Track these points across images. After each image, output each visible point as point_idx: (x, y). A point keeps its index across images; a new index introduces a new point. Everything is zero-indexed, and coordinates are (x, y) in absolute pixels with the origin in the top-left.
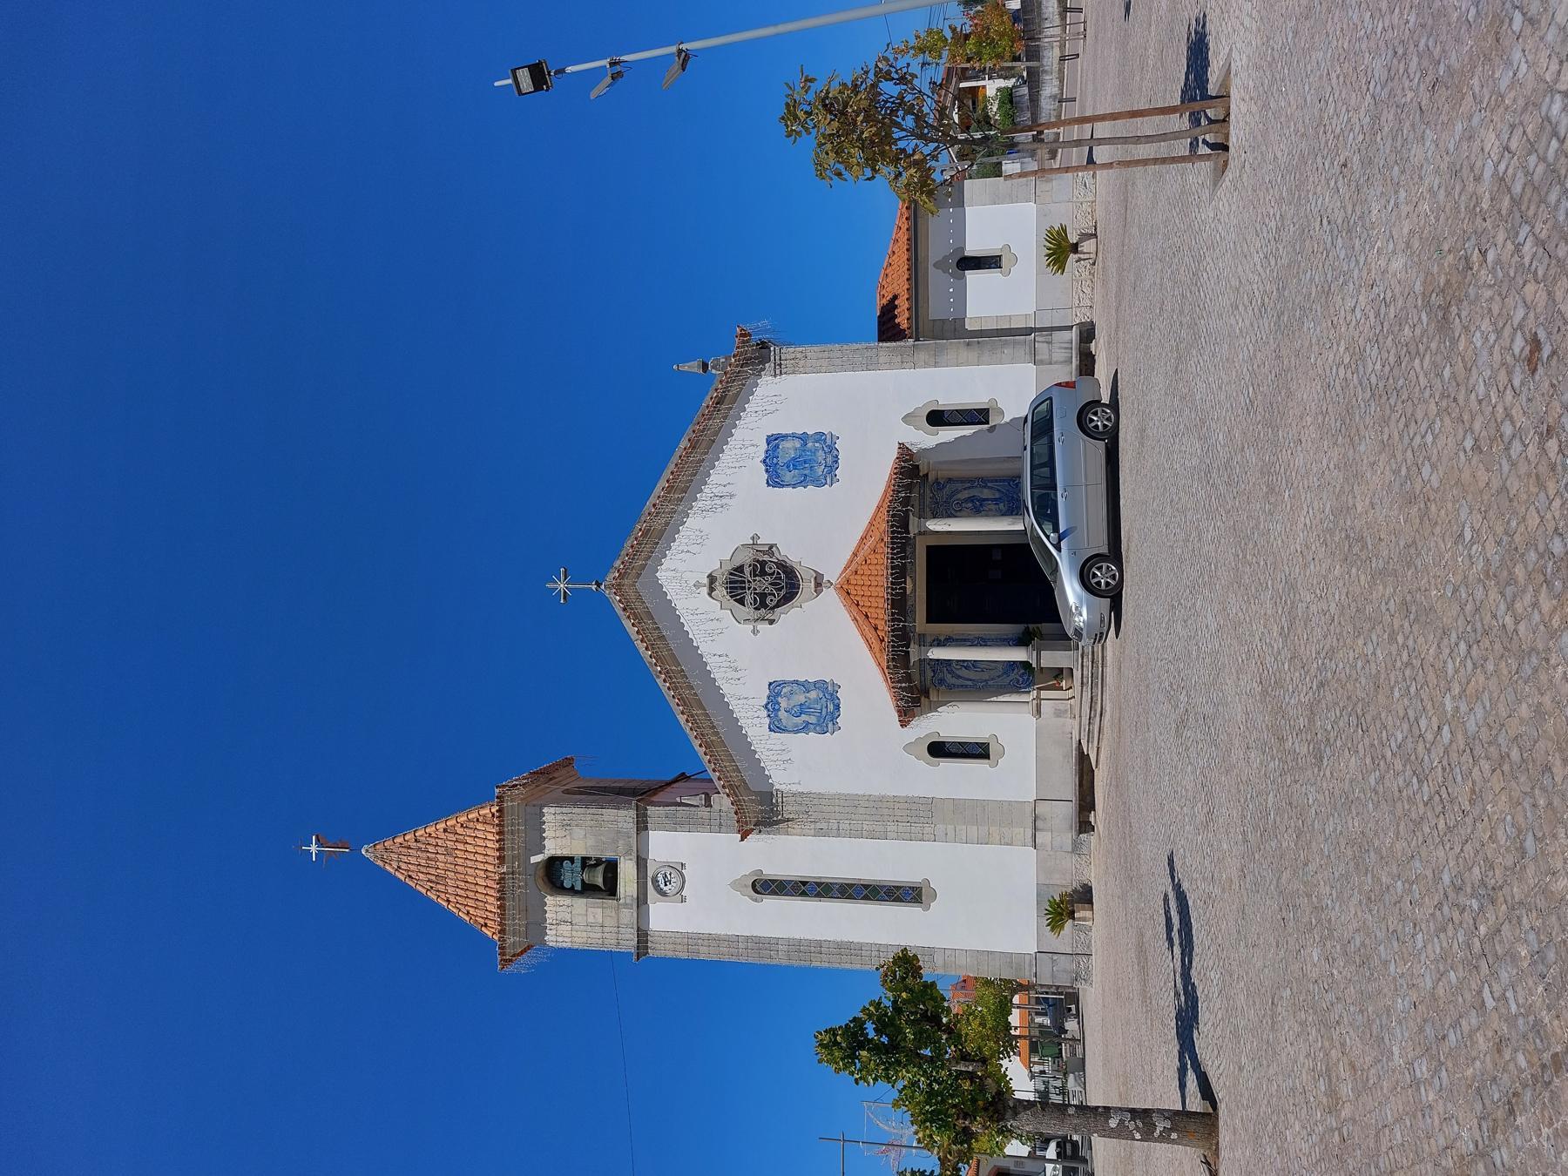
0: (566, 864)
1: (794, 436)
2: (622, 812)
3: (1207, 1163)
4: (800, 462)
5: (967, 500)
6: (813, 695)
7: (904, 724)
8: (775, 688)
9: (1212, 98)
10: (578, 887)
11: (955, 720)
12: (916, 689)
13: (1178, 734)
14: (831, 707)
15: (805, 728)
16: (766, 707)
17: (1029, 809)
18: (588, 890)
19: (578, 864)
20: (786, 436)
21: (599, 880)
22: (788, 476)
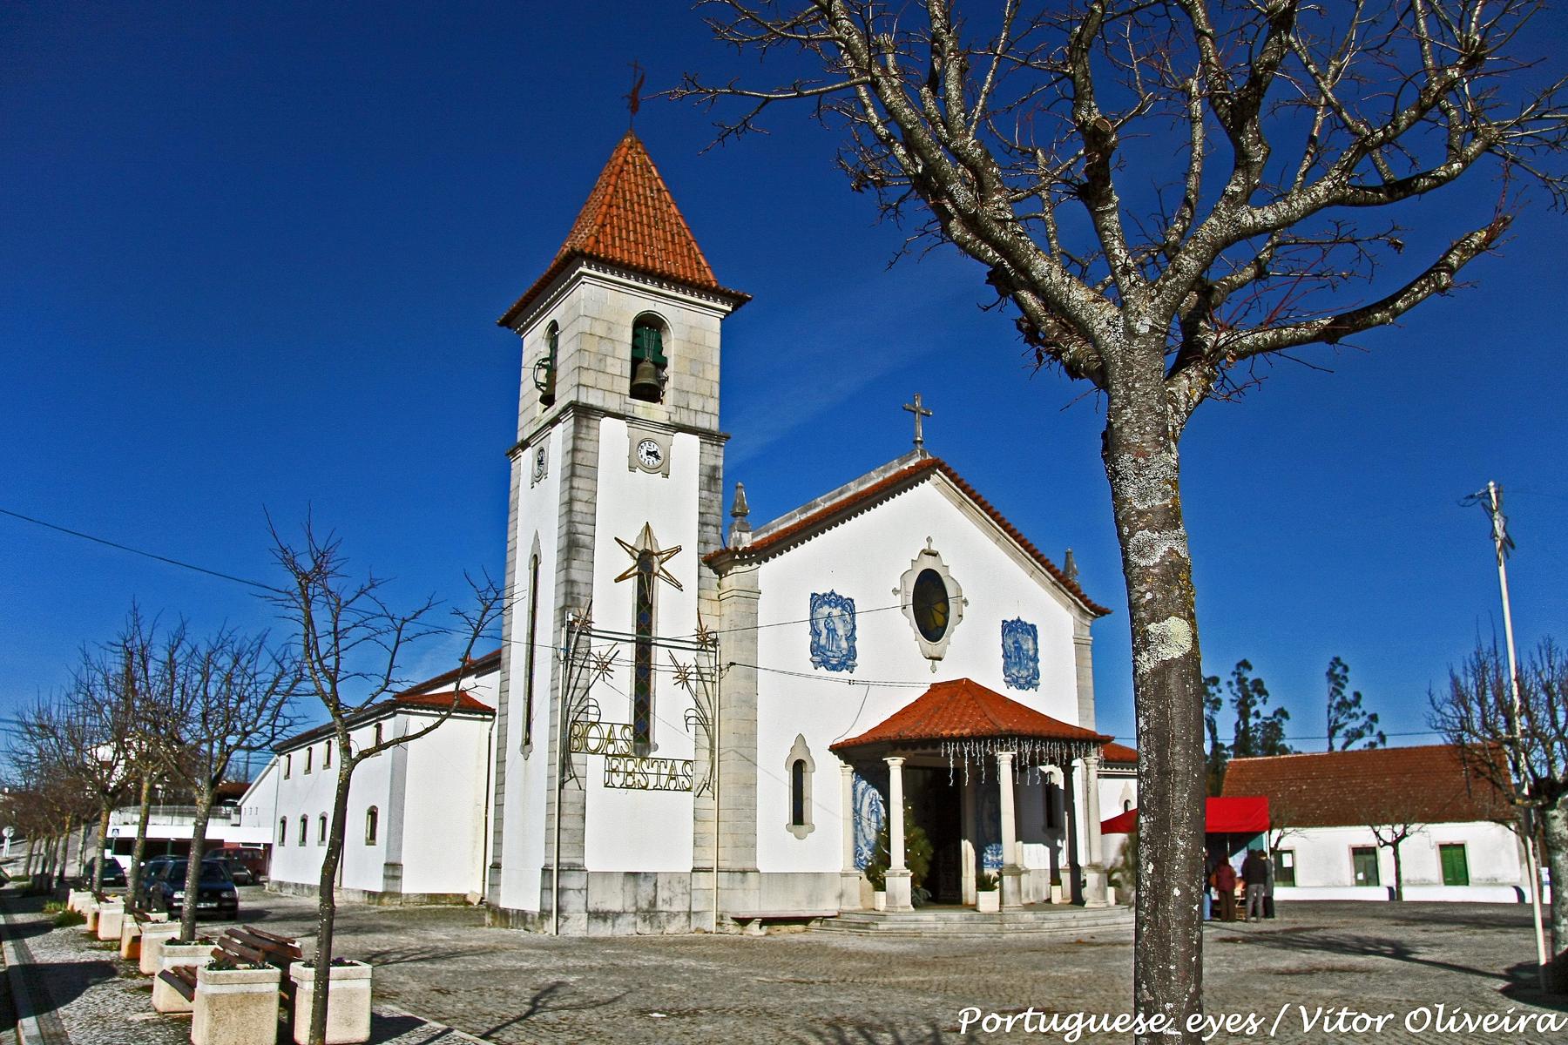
1: (1036, 650)
3: (703, 721)
6: (844, 644)
7: (837, 749)
8: (847, 605)
11: (832, 783)
12: (863, 756)
14: (834, 662)
15: (815, 633)
16: (832, 593)
17: (748, 865)
20: (1035, 643)
22: (1010, 642)
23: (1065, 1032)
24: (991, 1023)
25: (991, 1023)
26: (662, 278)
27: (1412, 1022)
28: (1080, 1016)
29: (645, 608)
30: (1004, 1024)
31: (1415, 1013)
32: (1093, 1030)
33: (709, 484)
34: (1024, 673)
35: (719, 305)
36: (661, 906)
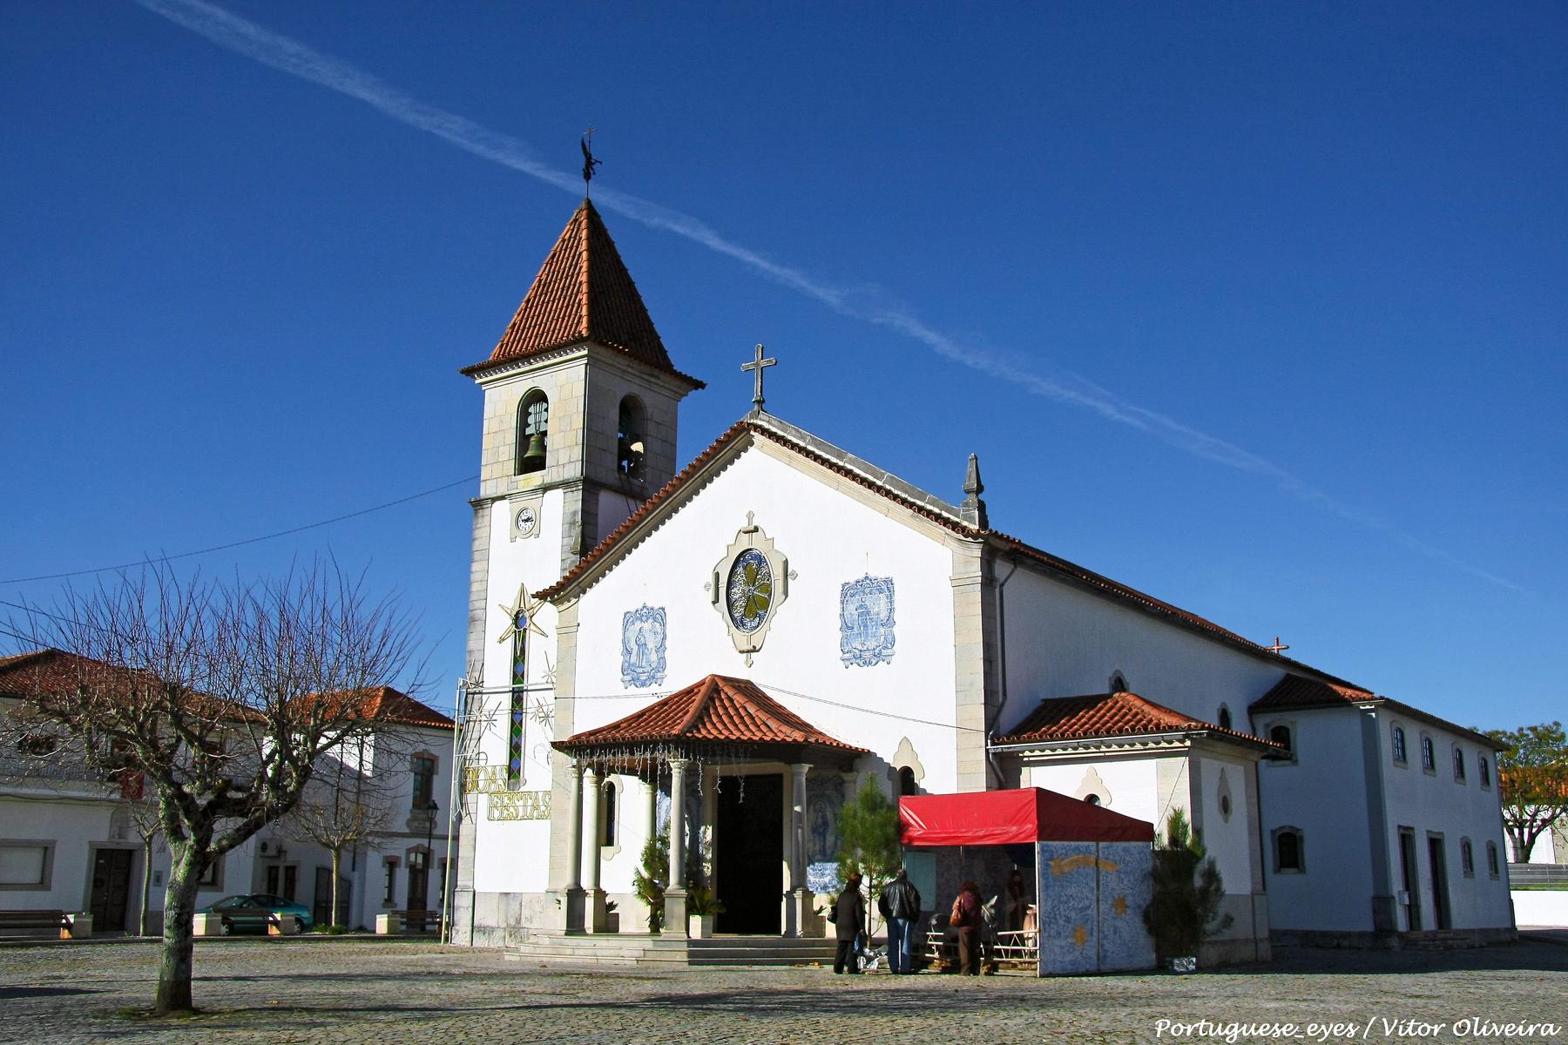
4: (866, 620)
5: (824, 817)
9: (197, 1011)
10: (529, 431)
14: (643, 677)
15: (627, 651)
18: (523, 440)
21: (531, 459)
24: (1177, 1030)
25: (1177, 1030)
26: (526, 357)
29: (519, 659)
34: (871, 644)
36: (524, 923)
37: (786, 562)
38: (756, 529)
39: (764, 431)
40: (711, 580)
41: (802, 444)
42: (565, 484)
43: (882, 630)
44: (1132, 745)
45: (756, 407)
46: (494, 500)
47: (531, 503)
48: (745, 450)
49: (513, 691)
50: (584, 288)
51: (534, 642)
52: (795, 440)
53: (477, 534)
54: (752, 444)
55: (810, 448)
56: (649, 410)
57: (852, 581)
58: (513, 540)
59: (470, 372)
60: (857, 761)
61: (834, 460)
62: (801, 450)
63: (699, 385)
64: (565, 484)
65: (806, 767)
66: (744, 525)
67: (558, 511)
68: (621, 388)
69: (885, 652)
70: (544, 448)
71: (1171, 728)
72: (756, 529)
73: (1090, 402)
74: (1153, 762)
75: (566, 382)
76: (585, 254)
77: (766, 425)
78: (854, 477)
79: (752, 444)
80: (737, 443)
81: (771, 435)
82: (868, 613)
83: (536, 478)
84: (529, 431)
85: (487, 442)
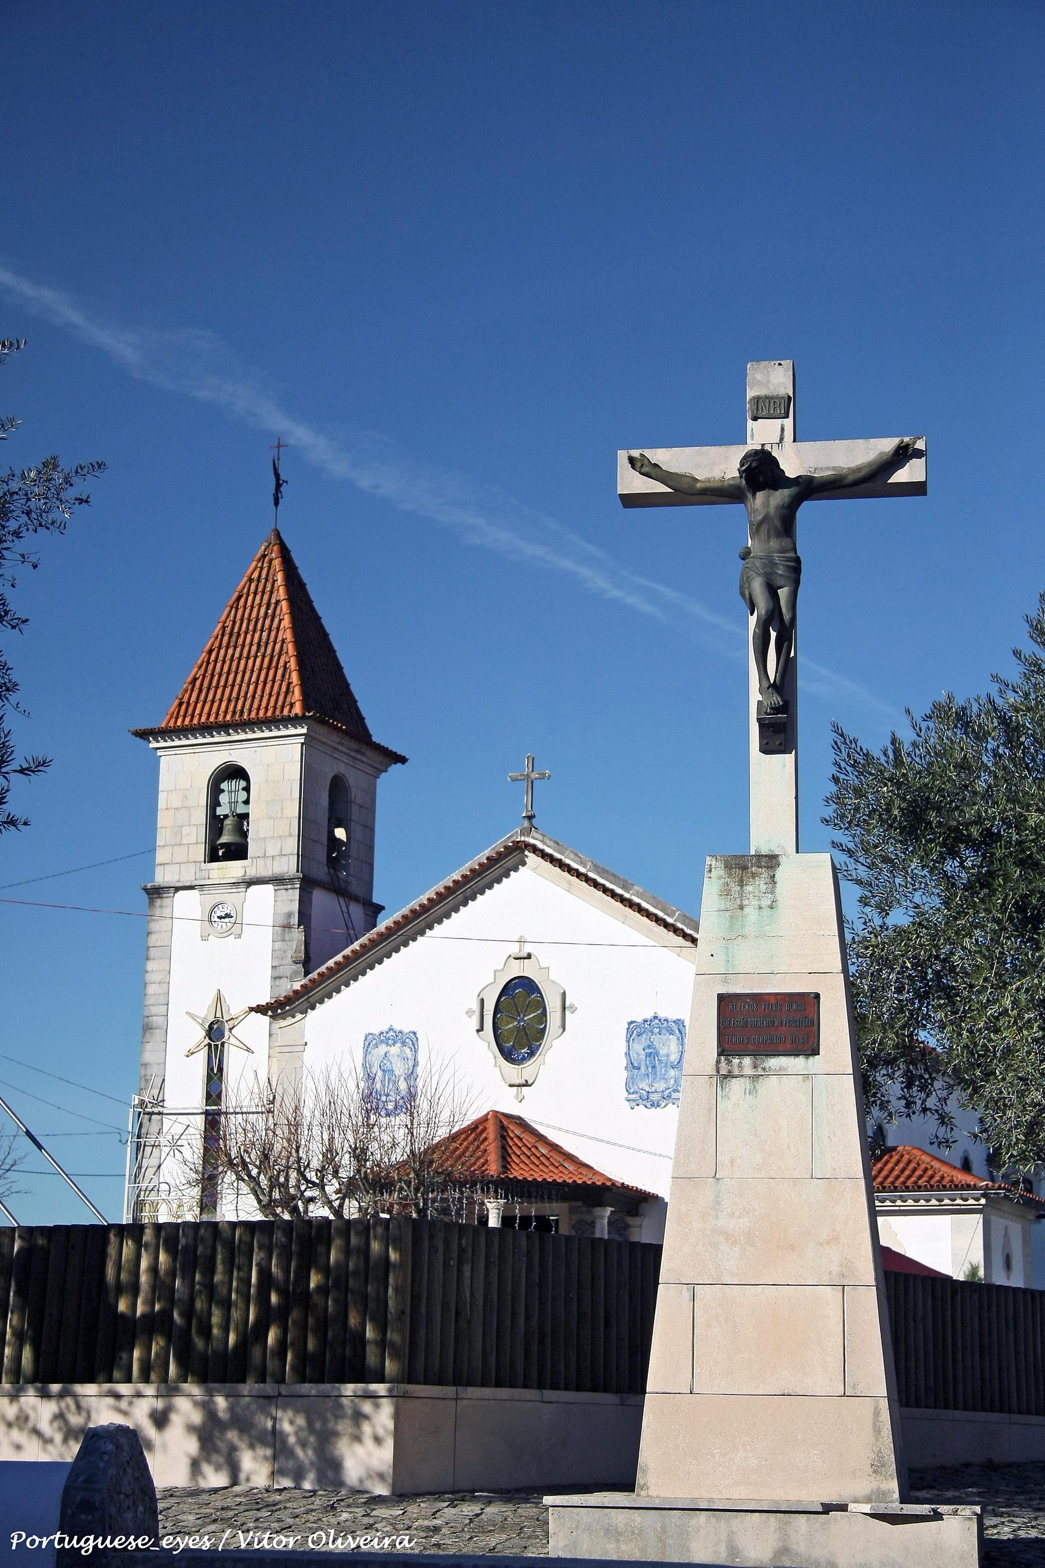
0: (243, 784)
2: (294, 860)
10: (220, 811)
13: (76, 499)
16: (655, 1017)
18: (215, 824)
19: (241, 809)
21: (226, 841)
22: (638, 1047)
23: (81, 1548)
24: (33, 1542)
25: (33, 1542)
26: (225, 727)
27: (313, 1542)
28: (92, 1537)
30: (41, 1543)
31: (315, 1535)
32: (100, 1546)
33: (283, 934)
34: (660, 1086)
35: (292, 731)
37: (564, 994)
38: (529, 956)
39: (535, 849)
40: (475, 1006)
41: (582, 870)
42: (278, 881)
43: (672, 1073)
44: (928, 1201)
45: (526, 823)
46: (177, 889)
47: (231, 900)
48: (516, 869)
49: (207, 1113)
50: (290, 648)
51: (234, 1060)
52: (574, 865)
53: (154, 926)
54: (524, 864)
55: (591, 875)
56: (353, 790)
57: (640, 1020)
58: (204, 938)
59: (144, 735)
60: (643, 1206)
61: (619, 891)
62: (579, 875)
63: (403, 760)
64: (278, 881)
65: (609, 1210)
66: (514, 949)
67: (266, 908)
68: (330, 768)
69: (675, 1095)
70: (245, 835)
71: (968, 1187)
72: (529, 956)
73: (567, 564)
74: (948, 1218)
75: (276, 764)
76: (284, 605)
77: (540, 845)
78: (640, 910)
79: (524, 864)
80: (508, 862)
81: (544, 855)
82: (657, 1054)
83: (234, 869)
84: (220, 811)
85: (163, 819)
